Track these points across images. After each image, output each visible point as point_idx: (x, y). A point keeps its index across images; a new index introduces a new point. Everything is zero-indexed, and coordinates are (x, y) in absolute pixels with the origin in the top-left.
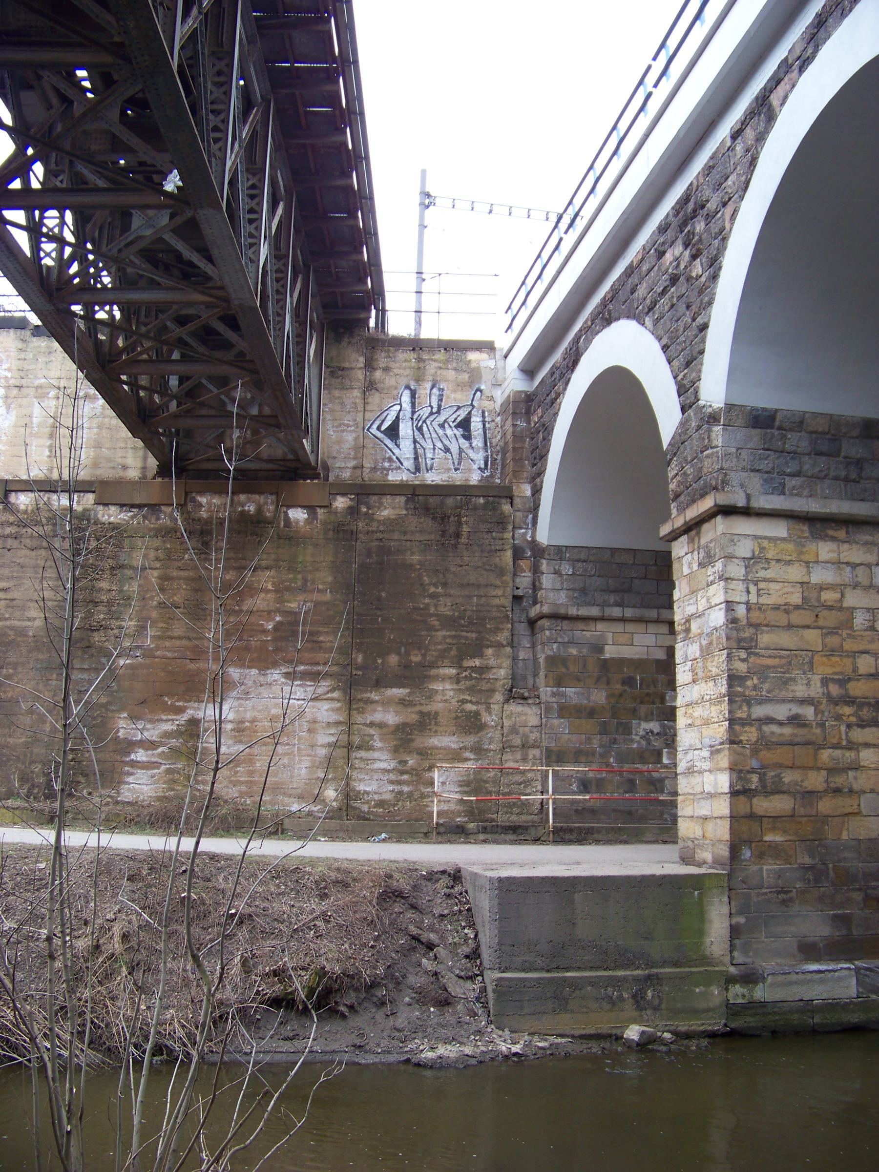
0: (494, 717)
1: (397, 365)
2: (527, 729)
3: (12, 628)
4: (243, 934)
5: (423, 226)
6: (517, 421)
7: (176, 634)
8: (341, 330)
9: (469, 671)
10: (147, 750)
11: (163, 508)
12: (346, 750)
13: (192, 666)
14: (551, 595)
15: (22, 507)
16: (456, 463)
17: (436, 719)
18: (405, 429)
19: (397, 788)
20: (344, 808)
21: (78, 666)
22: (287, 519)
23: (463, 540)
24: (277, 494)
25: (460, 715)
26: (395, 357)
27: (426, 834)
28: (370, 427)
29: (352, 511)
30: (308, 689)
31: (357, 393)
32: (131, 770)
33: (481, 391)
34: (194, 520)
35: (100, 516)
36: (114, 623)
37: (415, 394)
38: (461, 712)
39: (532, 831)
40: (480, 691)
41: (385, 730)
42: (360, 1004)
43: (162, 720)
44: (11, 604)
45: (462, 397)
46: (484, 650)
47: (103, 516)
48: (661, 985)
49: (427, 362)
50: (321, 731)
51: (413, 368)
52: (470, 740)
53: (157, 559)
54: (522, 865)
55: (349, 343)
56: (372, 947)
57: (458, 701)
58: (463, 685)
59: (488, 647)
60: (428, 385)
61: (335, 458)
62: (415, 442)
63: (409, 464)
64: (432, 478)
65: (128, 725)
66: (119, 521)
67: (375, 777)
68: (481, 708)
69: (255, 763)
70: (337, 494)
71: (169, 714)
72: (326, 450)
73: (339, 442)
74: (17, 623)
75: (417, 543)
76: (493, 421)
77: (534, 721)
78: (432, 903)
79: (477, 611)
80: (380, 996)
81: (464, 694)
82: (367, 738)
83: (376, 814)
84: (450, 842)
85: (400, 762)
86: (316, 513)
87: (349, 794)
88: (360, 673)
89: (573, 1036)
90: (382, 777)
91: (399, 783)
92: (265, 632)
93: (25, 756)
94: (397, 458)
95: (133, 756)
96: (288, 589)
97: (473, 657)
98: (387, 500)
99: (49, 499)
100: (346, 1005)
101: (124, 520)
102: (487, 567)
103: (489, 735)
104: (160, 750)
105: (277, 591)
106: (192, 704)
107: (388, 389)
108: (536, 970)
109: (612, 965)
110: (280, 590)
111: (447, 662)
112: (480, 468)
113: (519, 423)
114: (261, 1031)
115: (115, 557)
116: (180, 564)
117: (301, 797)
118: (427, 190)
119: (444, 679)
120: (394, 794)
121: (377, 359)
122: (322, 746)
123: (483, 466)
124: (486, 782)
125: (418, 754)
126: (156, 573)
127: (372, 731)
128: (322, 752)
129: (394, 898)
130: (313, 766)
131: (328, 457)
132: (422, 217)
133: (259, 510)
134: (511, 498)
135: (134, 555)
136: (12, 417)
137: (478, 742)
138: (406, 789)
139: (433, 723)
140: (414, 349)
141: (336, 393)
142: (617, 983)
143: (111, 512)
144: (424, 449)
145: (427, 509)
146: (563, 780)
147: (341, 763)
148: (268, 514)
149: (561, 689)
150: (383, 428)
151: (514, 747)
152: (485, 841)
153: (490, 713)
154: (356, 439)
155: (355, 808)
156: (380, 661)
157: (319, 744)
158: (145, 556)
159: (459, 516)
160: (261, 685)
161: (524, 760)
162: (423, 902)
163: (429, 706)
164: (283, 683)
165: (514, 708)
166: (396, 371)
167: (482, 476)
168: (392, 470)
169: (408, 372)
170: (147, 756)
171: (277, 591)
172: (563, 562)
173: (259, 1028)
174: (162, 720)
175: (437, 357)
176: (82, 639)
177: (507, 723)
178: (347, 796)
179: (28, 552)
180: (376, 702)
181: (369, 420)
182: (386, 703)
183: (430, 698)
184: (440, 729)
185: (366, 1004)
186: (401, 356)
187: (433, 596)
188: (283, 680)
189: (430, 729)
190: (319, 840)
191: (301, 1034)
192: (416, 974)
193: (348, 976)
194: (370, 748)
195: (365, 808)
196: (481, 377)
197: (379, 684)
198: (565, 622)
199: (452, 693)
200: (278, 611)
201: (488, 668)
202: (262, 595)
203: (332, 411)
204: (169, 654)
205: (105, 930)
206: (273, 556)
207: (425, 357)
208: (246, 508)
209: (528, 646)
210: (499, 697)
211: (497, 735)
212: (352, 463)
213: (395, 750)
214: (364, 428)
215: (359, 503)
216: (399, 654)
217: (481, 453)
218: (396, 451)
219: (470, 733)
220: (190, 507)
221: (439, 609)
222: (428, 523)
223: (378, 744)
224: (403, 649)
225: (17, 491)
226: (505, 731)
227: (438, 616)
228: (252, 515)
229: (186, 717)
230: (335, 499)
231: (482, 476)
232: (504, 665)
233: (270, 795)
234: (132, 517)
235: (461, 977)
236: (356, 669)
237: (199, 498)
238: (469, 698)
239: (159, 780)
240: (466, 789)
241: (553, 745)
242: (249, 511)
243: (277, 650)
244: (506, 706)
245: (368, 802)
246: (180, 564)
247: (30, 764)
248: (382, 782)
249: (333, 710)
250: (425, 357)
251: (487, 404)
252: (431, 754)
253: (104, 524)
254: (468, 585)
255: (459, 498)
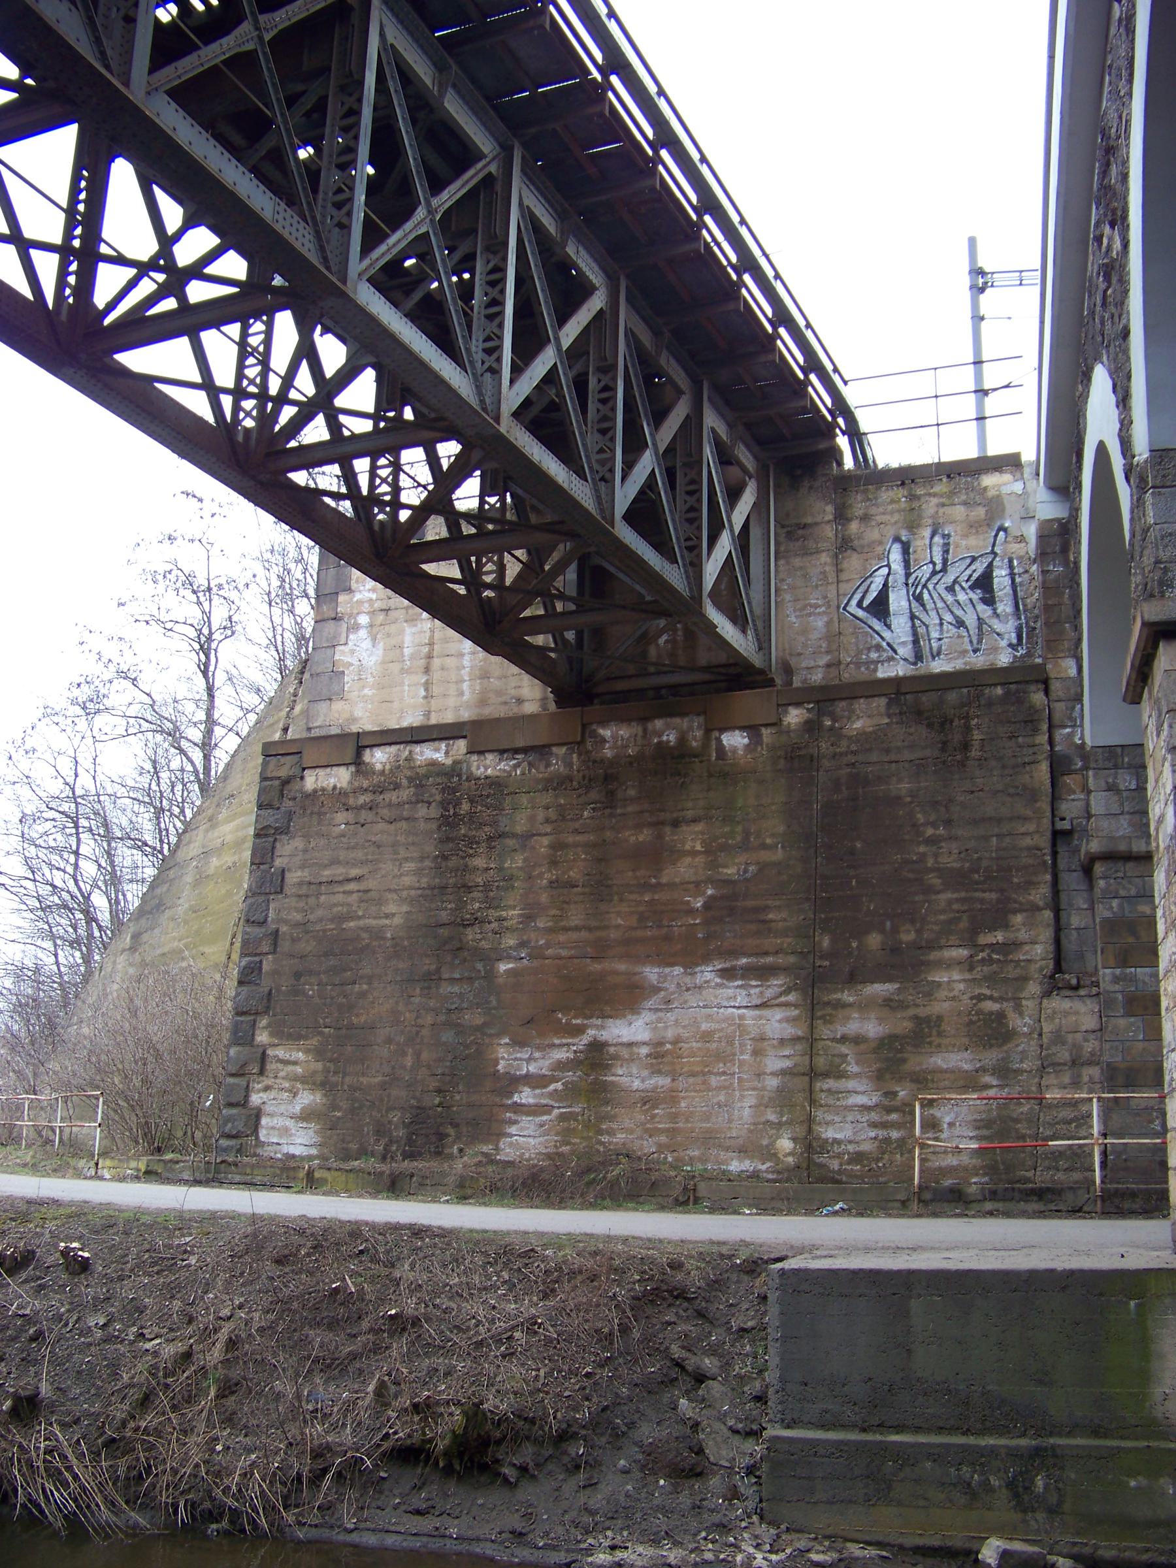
0: (1027, 1020)
1: (881, 510)
2: (1079, 1036)
3: (367, 929)
4: (399, 1346)
5: (978, 318)
6: (1048, 565)
7: (573, 924)
8: (799, 472)
9: (987, 951)
10: (534, 1088)
11: (554, 749)
12: (807, 1078)
13: (597, 967)
14: (1104, 824)
15: (378, 767)
16: (975, 642)
17: (939, 1026)
18: (898, 601)
19: (882, 1133)
20: (804, 1165)
21: (446, 976)
22: (720, 748)
23: (975, 753)
24: (705, 713)
25: (975, 1018)
26: (876, 498)
27: (904, 1203)
28: (847, 604)
29: (811, 727)
30: (752, 991)
31: (825, 558)
32: (514, 1117)
33: (1005, 530)
34: (595, 762)
35: (474, 769)
36: (493, 914)
37: (909, 548)
38: (977, 1014)
39: (1069, 1196)
40: (1006, 980)
41: (863, 1047)
42: (537, 1465)
43: (554, 1045)
44: (366, 897)
45: (978, 543)
46: (1011, 916)
47: (478, 768)
48: (1062, 1468)
49: (923, 500)
50: (771, 1052)
51: (904, 510)
52: (991, 1057)
53: (547, 821)
54: (867, 1250)
55: (811, 488)
56: (588, 1375)
57: (971, 998)
58: (978, 972)
59: (1015, 912)
60: (927, 533)
61: (800, 654)
62: (913, 617)
63: (905, 651)
64: (939, 666)
65: (510, 1054)
66: (498, 774)
67: (850, 1118)
68: (1008, 1006)
69: (679, 1102)
70: (790, 704)
71: (563, 1037)
72: (787, 646)
73: (805, 631)
74: (373, 922)
75: (907, 765)
76: (1026, 572)
77: (1089, 1022)
78: (734, 1310)
79: (998, 859)
80: (573, 1454)
81: (980, 986)
82: (837, 1060)
83: (851, 1174)
84: (935, 1215)
85: (886, 1094)
86: (760, 735)
87: (810, 1145)
88: (827, 963)
89: (901, 1547)
90: (859, 1117)
91: (884, 1125)
92: (691, 912)
93: (382, 1100)
94: (888, 644)
95: (516, 1098)
96: (724, 848)
97: (993, 929)
98: (860, 705)
99: (410, 752)
100: (514, 1465)
101: (504, 771)
102: (1012, 791)
103: (1020, 1048)
104: (552, 1087)
105: (707, 852)
106: (595, 1021)
107: (869, 546)
108: (844, 1427)
109: (979, 1426)
110: (714, 852)
111: (953, 939)
112: (1010, 645)
113: (1051, 568)
114: (383, 1497)
115: (494, 823)
116: (577, 825)
117: (743, 1151)
118: (980, 265)
119: (949, 965)
120: (877, 1144)
121: (851, 505)
122: (773, 1074)
123: (1015, 641)
124: (1017, 1121)
125: (912, 1081)
126: (545, 841)
127: (844, 1049)
128: (773, 1083)
129: (670, 1300)
130: (760, 1105)
131: (791, 655)
132: (975, 305)
133: (682, 739)
134: (1046, 683)
135: (518, 819)
136: (379, 651)
137: (1003, 1059)
138: (895, 1134)
139: (934, 1033)
140: (903, 484)
141: (797, 562)
142: (980, 1458)
143: (488, 762)
144: (927, 627)
145: (919, 713)
146: (1138, 1115)
147: (800, 1098)
148: (694, 744)
149: (1128, 970)
150: (866, 603)
151: (1060, 1064)
152: (991, 1214)
153: (1021, 1014)
154: (828, 624)
155: (821, 1166)
156: (854, 945)
157: (768, 1071)
158: (532, 819)
159: (967, 718)
160: (688, 990)
161: (1076, 1084)
162: (718, 1307)
163: (928, 1008)
164: (717, 985)
165: (1058, 1003)
166: (879, 518)
167: (1015, 656)
168: (882, 662)
169: (896, 517)
170: (535, 1096)
171: (707, 852)
172: (1120, 771)
173: (381, 1492)
174: (554, 1045)
175: (937, 489)
176: (451, 938)
177: (1047, 1028)
178: (809, 1148)
179: (382, 826)
180: (850, 1005)
181: (845, 595)
182: (864, 1007)
183: (929, 995)
184: (945, 1041)
185: (550, 1466)
186: (885, 495)
187: (932, 841)
188: (718, 980)
189: (930, 1043)
190: (744, 1214)
191: (438, 1506)
192: (658, 1423)
193: (526, 1419)
194: (841, 1075)
195: (835, 1165)
196: (1003, 510)
197: (853, 979)
198: (1130, 865)
199: (962, 986)
200: (711, 881)
201: (1016, 945)
202: (688, 860)
203: (793, 588)
204: (564, 953)
205: (208, 1333)
206: (701, 803)
207: (920, 491)
208: (665, 738)
209: (1085, 906)
210: (1033, 988)
211: (1033, 1047)
212: (824, 660)
213: (879, 1077)
214: (838, 607)
215: (821, 713)
216: (882, 931)
217: (1010, 622)
218: (886, 634)
219: (991, 1046)
220: (589, 746)
221: (940, 860)
222: (921, 732)
223: (854, 1068)
224: (888, 924)
225: (372, 746)
226: (1045, 1040)
227: (939, 871)
228: (671, 748)
229: (585, 1039)
230: (786, 712)
231: (1015, 656)
232: (1042, 938)
233: (699, 1148)
234: (515, 767)
235: (736, 1432)
236: (821, 958)
237: (601, 731)
238: (988, 992)
239: (550, 1130)
240: (985, 1132)
241: (1119, 1059)
242: (668, 741)
243: (709, 937)
244: (1045, 1001)
245: (839, 1156)
246: (577, 825)
247: (387, 1112)
248: (860, 1126)
249: (787, 1020)
250: (920, 491)
251: (1015, 548)
252: (933, 1081)
253: (479, 779)
254: (983, 820)
255: (965, 690)
